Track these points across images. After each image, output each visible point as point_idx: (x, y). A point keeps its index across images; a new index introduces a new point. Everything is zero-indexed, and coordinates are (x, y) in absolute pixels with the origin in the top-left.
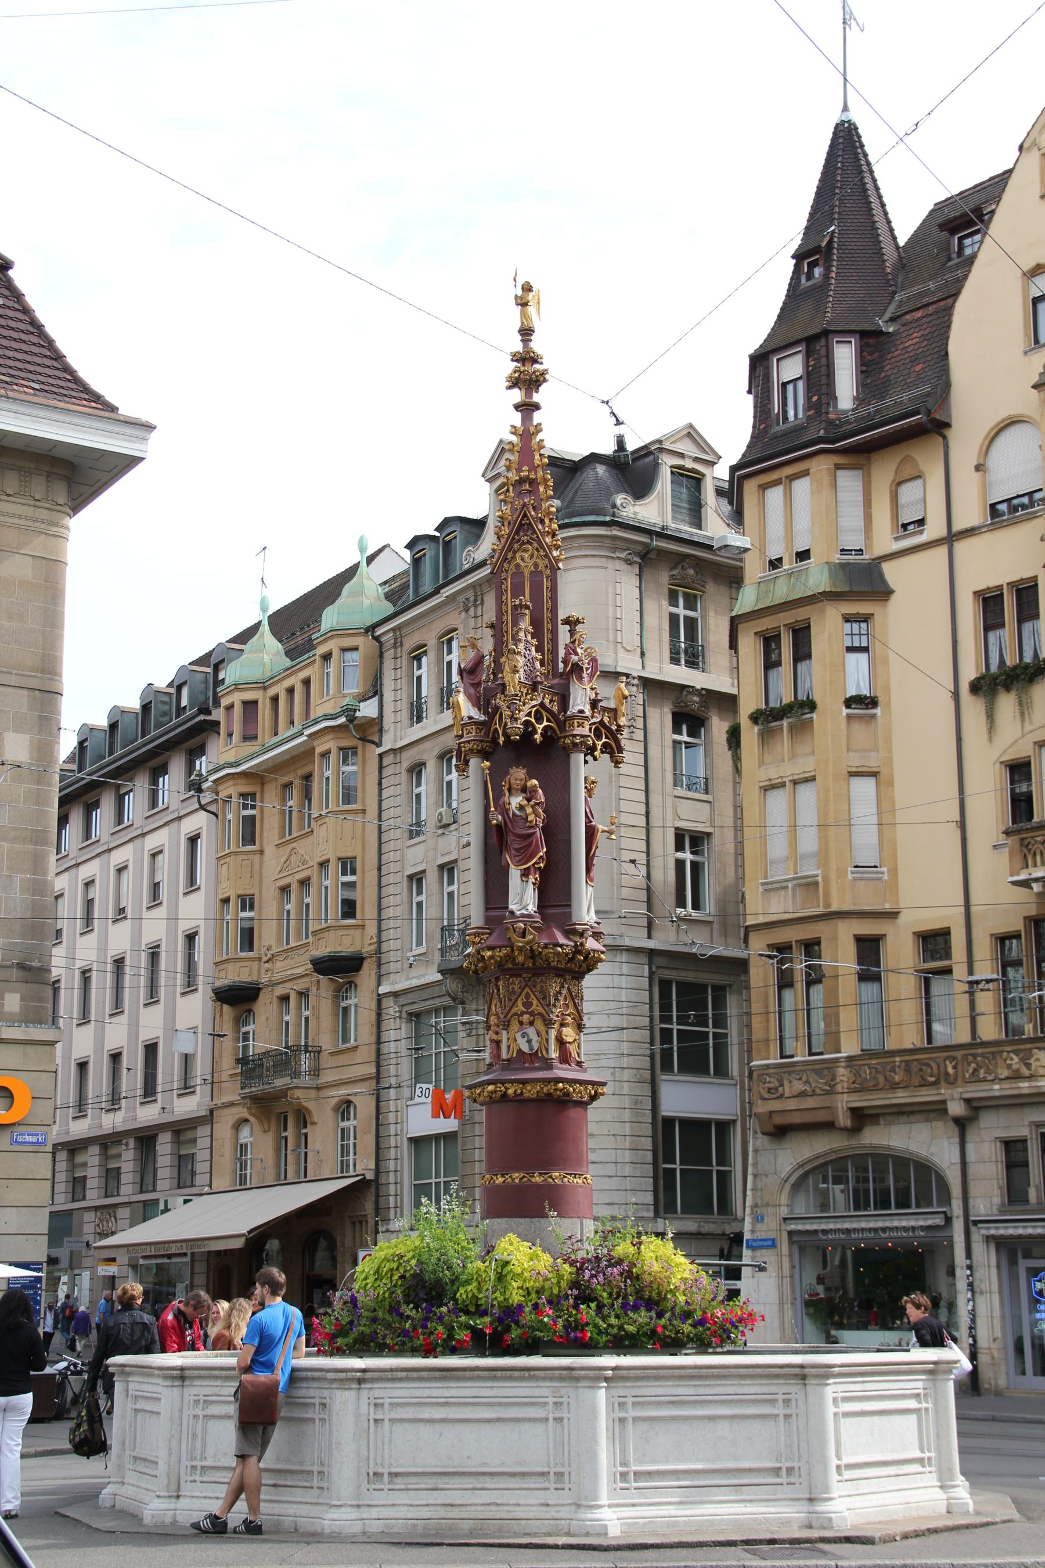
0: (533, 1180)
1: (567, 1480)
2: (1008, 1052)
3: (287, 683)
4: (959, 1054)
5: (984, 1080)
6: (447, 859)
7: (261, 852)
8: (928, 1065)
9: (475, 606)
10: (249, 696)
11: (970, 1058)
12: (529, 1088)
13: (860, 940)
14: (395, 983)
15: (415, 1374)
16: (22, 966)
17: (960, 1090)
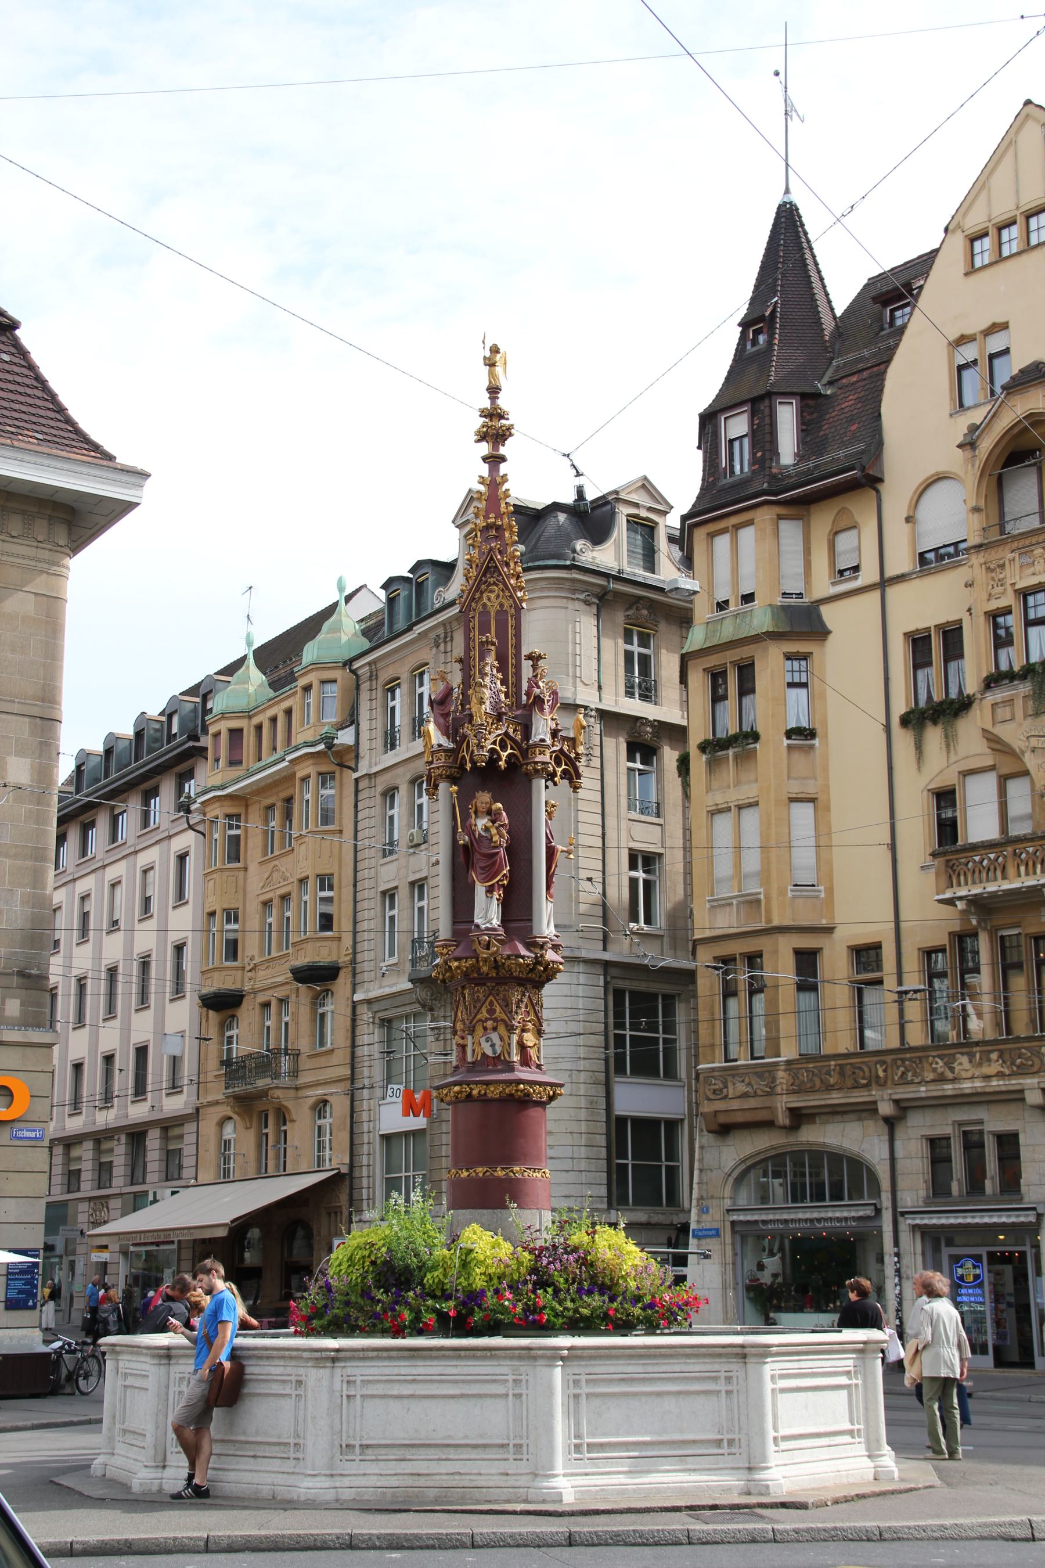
0: (496, 1174)
1: (525, 1452)
2: (934, 1057)
3: (270, 713)
4: (889, 1059)
5: (912, 1083)
6: (417, 876)
7: (246, 869)
8: (861, 1069)
9: (445, 642)
10: (235, 724)
11: (899, 1062)
12: (492, 1089)
13: (798, 953)
14: (368, 991)
15: (385, 1354)
16: (21, 974)
17: (890, 1091)
